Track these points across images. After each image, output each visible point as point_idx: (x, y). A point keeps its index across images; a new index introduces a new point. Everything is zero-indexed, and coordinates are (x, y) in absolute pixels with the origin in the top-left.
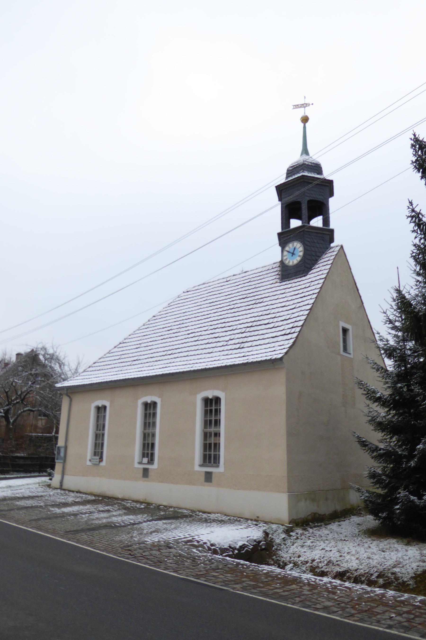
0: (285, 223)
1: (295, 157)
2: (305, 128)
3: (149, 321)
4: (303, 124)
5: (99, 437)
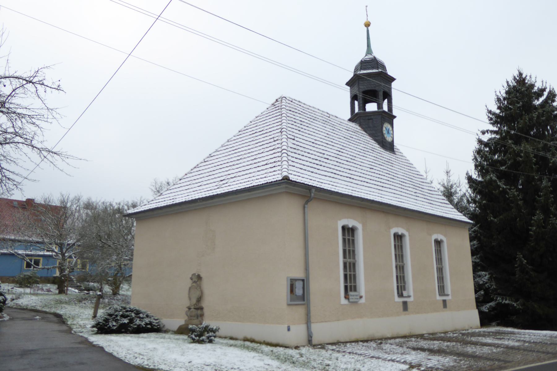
2: (368, 31)
3: (228, 141)
4: (366, 28)
5: (350, 268)
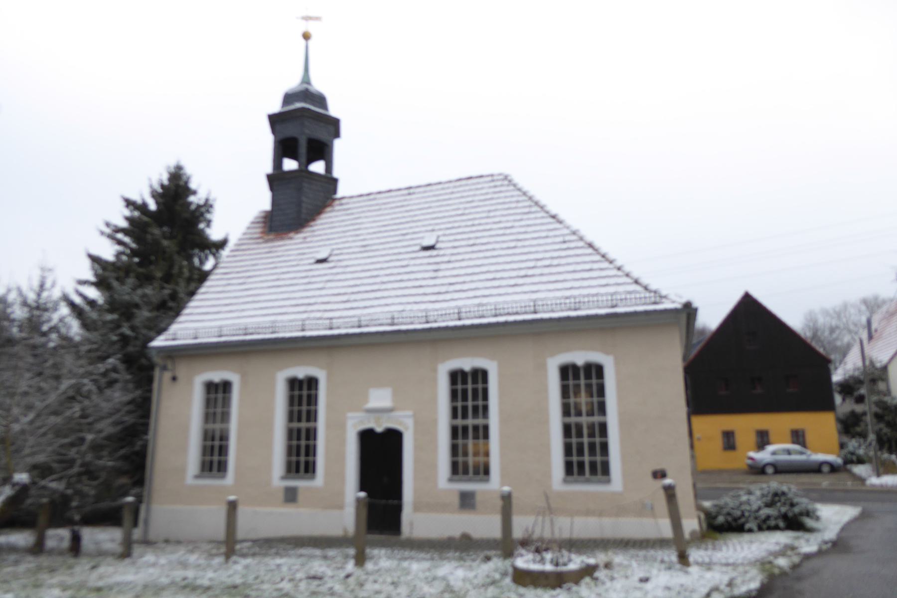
0: (278, 164)
1: (293, 83)
